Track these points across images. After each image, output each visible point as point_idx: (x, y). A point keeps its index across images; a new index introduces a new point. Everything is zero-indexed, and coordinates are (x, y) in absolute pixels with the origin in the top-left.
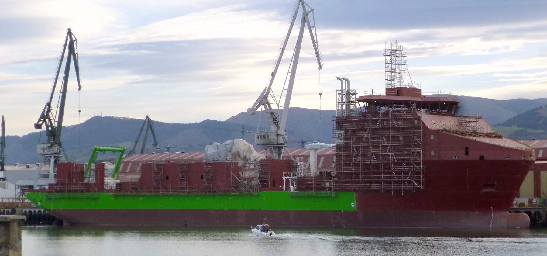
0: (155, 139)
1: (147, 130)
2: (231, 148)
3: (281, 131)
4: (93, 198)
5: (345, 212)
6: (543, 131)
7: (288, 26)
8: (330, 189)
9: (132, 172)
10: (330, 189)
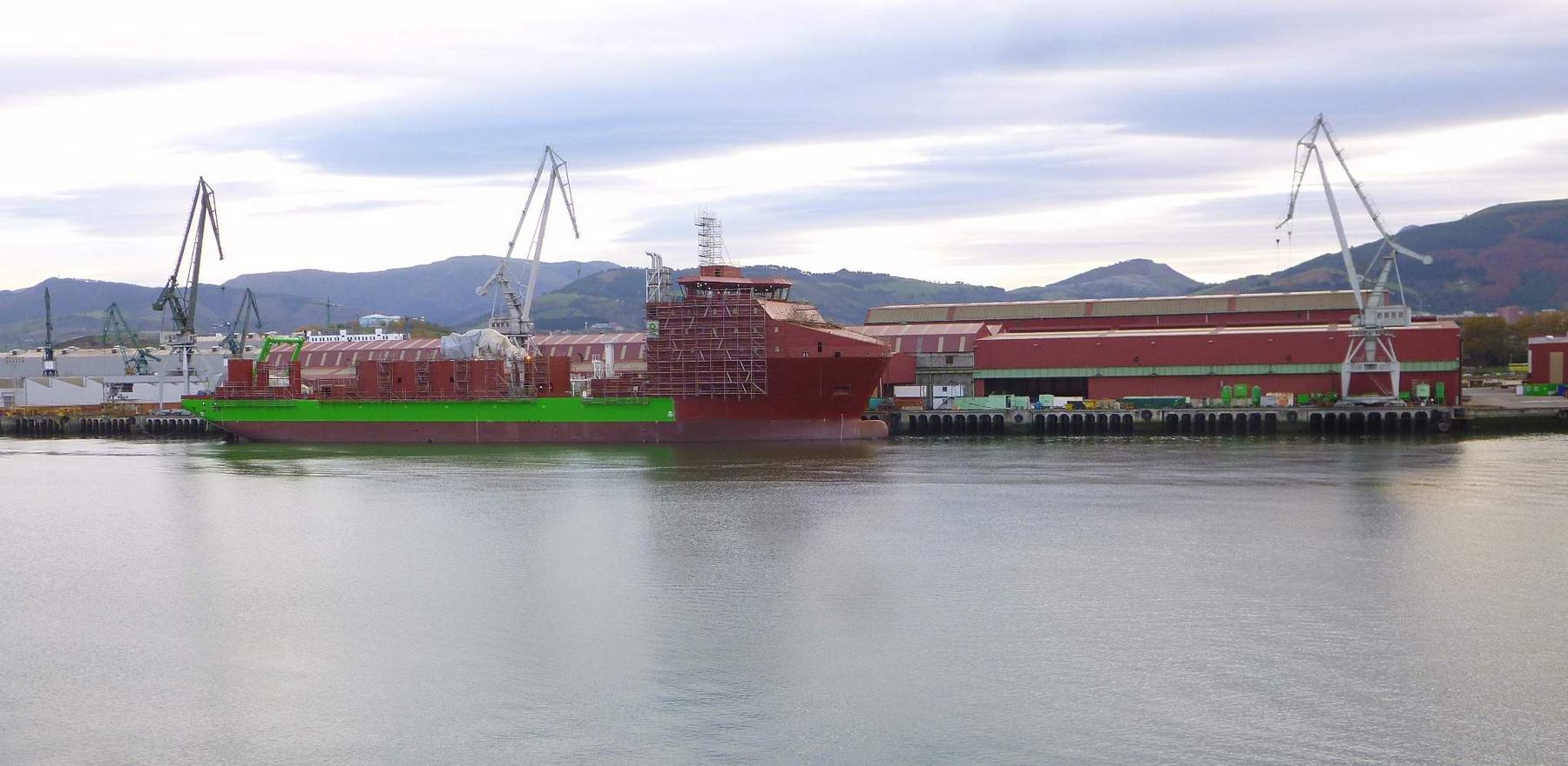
7: (1330, 180)
9: (344, 365)
10: (639, 395)
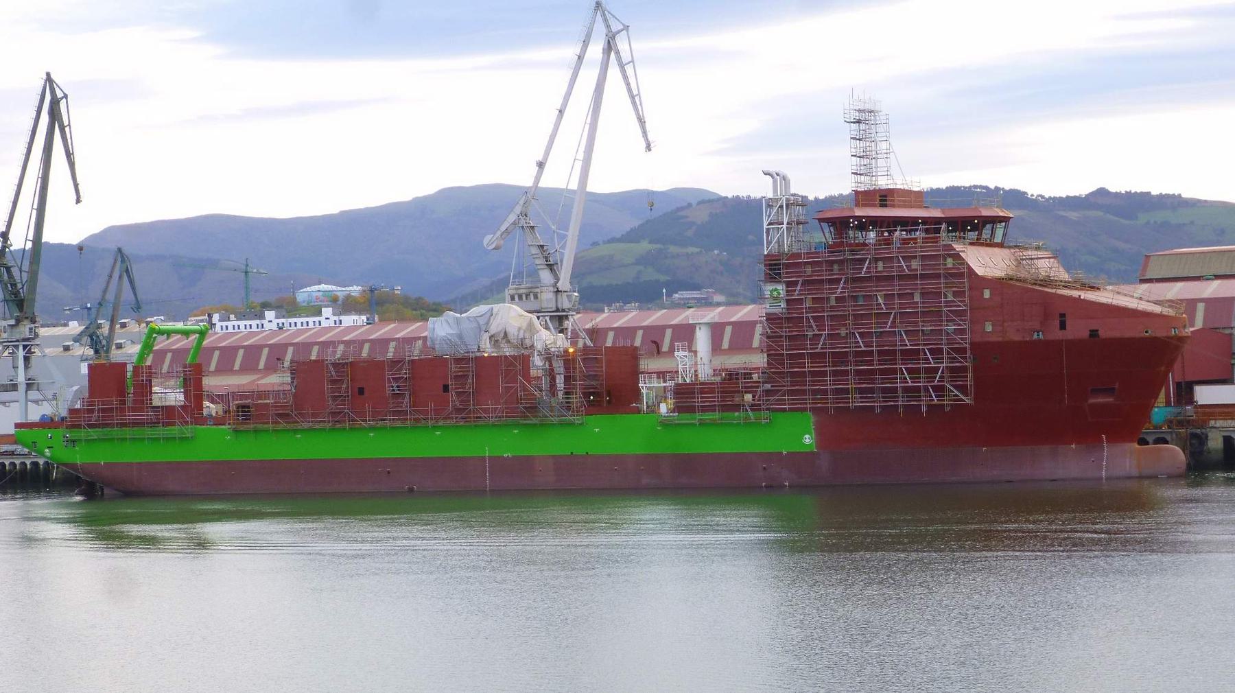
0: (135, 295)
1: (120, 277)
2: (488, 323)
3: (564, 284)
4: (181, 439)
5: (790, 454)
6: (698, 250)
8: (755, 407)
10: (755, 407)
